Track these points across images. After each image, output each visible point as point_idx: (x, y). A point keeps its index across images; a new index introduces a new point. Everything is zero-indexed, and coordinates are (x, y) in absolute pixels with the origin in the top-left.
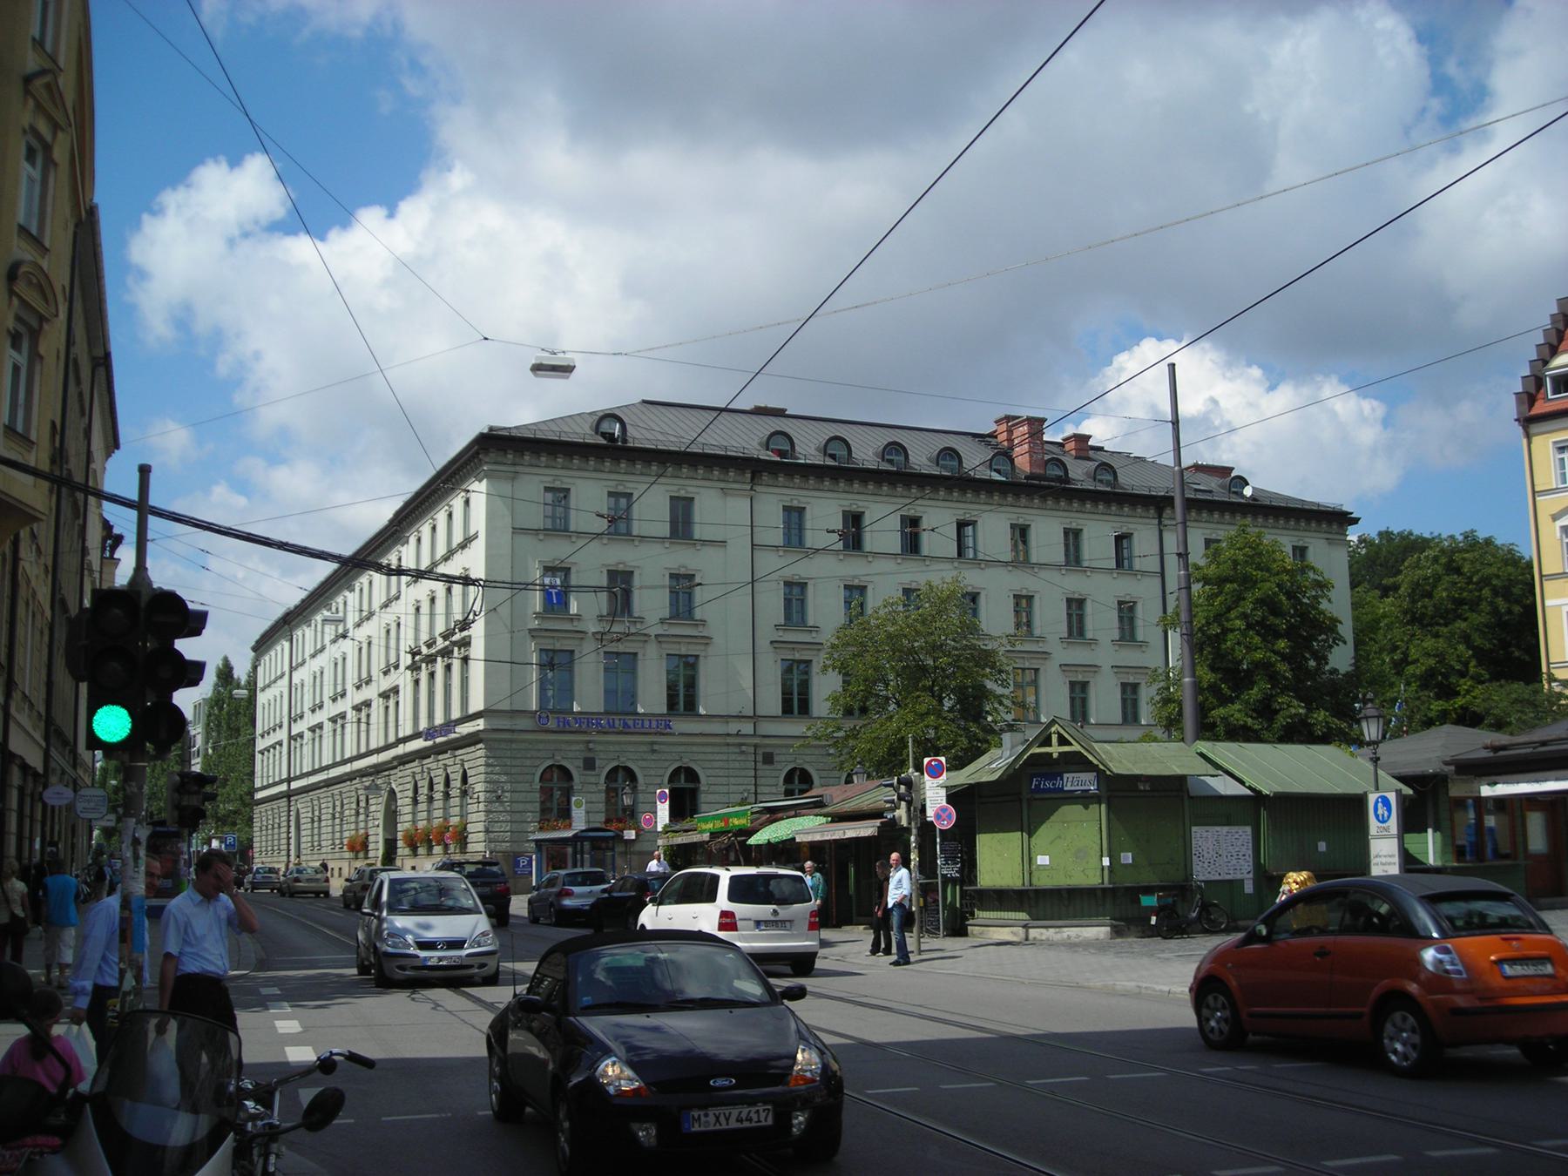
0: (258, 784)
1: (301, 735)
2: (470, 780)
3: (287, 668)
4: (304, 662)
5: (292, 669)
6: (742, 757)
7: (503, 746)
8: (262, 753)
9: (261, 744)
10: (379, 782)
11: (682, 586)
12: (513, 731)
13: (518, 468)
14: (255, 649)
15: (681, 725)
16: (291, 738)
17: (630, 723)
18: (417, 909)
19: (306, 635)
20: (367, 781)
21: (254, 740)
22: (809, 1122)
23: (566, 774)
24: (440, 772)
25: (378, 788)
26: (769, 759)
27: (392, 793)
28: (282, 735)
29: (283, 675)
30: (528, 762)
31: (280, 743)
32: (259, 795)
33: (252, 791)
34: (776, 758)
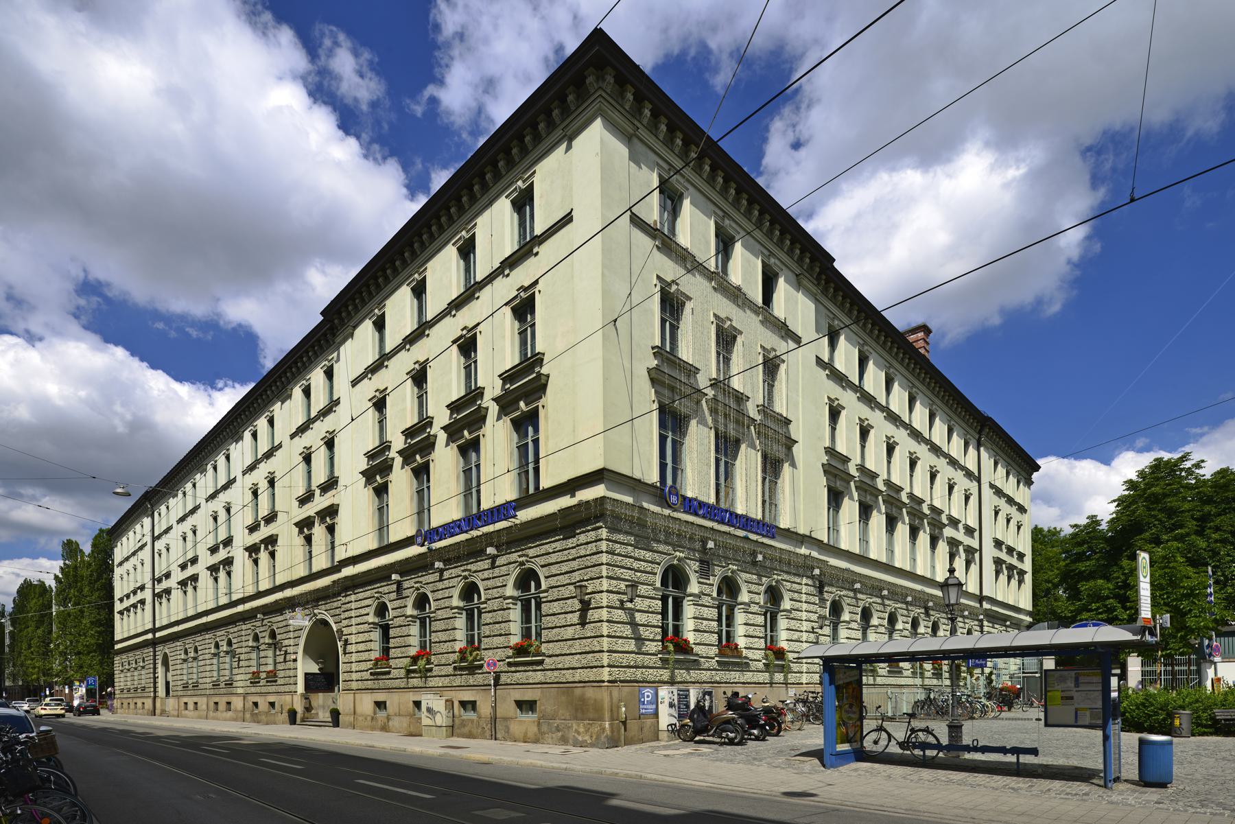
0: (117, 637)
3: (148, 539)
5: (155, 539)
8: (121, 613)
9: (118, 607)
14: (571, 220)
18: (1087, 580)
31: (142, 602)
32: (117, 647)
33: (113, 642)
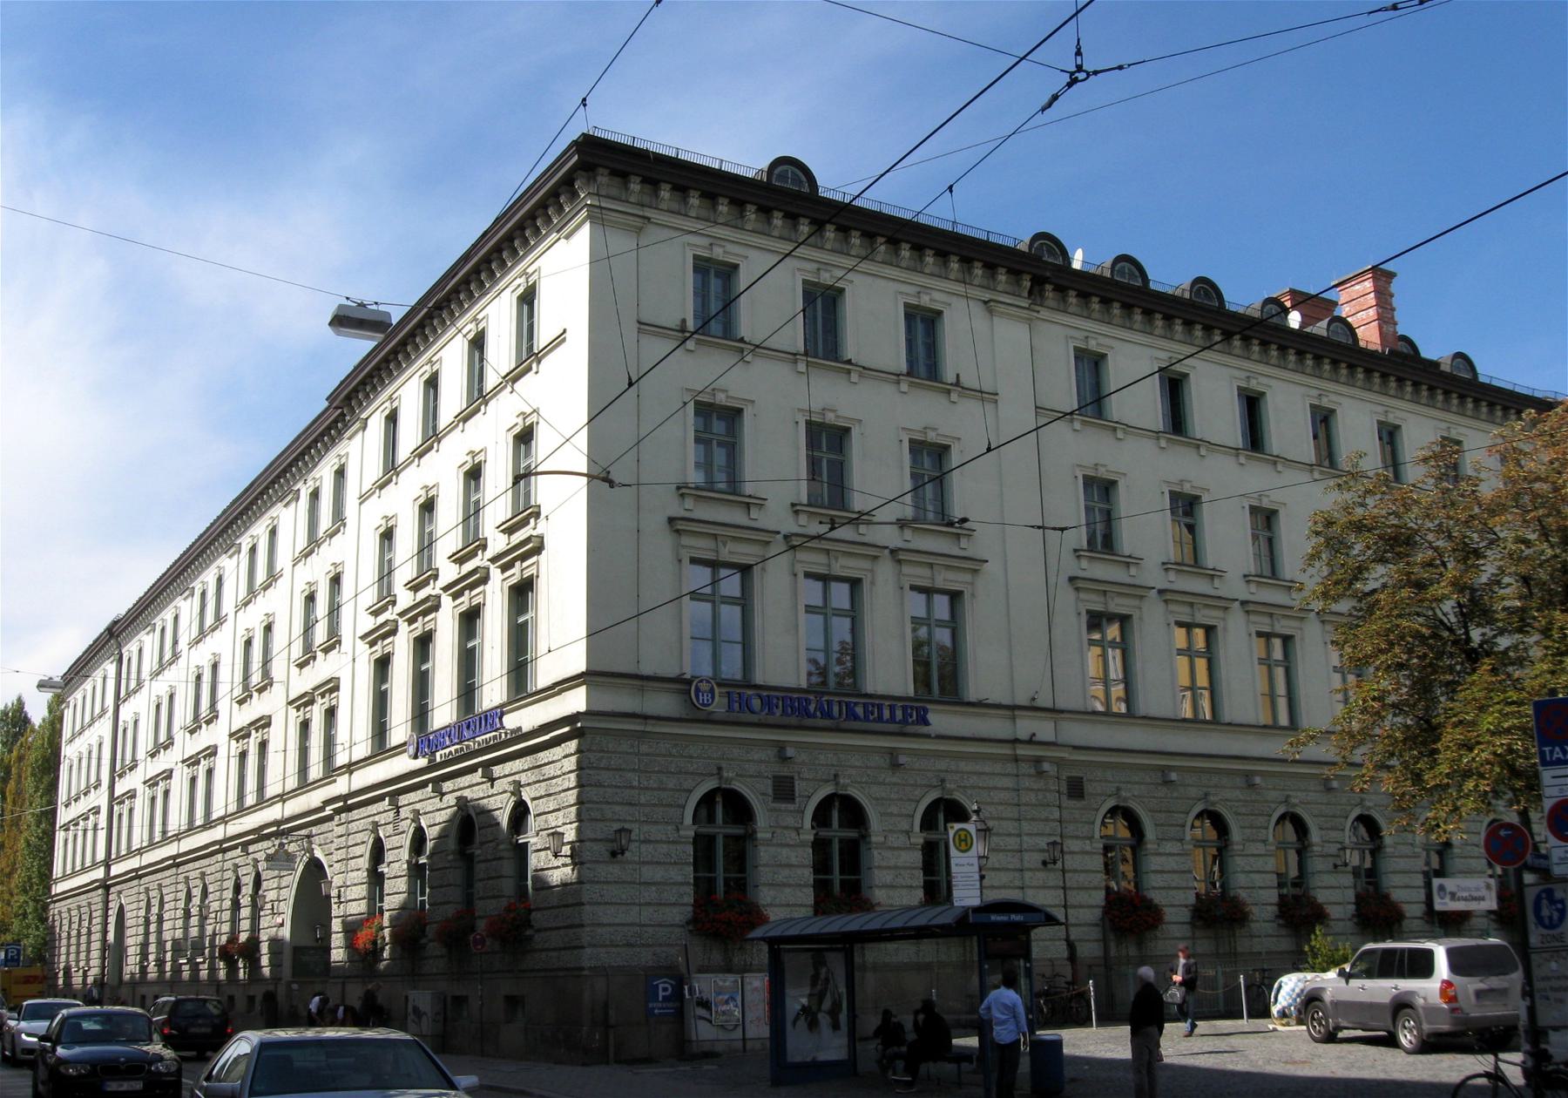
1: (131, 794)
2: (265, 885)
4: (140, 684)
6: (1040, 784)
7: (625, 746)
8: (66, 828)
9: (64, 816)
10: (292, 848)
11: (931, 460)
12: (646, 717)
13: (648, 213)
15: (942, 720)
16: (112, 798)
17: (859, 710)
19: (145, 644)
20: (268, 847)
21: (54, 812)
22: (71, 1077)
23: (738, 808)
24: (250, 869)
25: (290, 858)
26: (1076, 789)
27: (315, 870)
28: (100, 798)
29: (104, 711)
30: (671, 783)
34: (1089, 788)
